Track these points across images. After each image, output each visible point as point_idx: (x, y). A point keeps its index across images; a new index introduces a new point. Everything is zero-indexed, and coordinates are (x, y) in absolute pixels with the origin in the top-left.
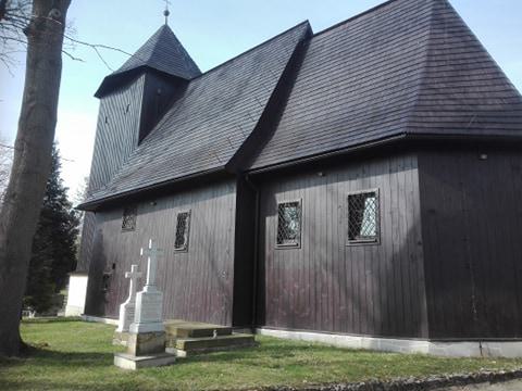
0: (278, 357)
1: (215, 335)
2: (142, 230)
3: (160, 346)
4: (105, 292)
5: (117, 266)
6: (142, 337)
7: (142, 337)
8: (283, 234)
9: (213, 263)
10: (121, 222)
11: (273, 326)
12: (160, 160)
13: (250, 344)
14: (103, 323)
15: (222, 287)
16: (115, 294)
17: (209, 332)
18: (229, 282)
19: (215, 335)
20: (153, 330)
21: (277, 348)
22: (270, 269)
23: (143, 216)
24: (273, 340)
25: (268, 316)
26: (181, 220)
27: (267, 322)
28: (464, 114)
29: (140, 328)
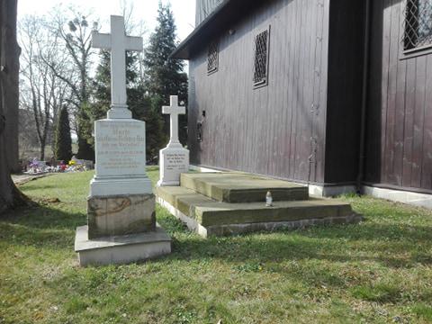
0: (397, 264)
1: (269, 200)
2: (224, 69)
3: (142, 221)
4: (199, 141)
5: (207, 112)
6: (100, 203)
7: (100, 203)
8: (410, 39)
9: (298, 95)
10: (205, 64)
11: (393, 183)
12: (306, 82)
13: (337, 220)
14: (199, 172)
15: (312, 126)
16: (207, 143)
17: (258, 195)
18: (321, 120)
19: (269, 200)
20: (124, 191)
21: (394, 233)
22: (389, 94)
23: (225, 51)
24: (394, 209)
25: (385, 168)
26: (262, 43)
27: (383, 177)
28: (361, 157)
29: (92, 194)
